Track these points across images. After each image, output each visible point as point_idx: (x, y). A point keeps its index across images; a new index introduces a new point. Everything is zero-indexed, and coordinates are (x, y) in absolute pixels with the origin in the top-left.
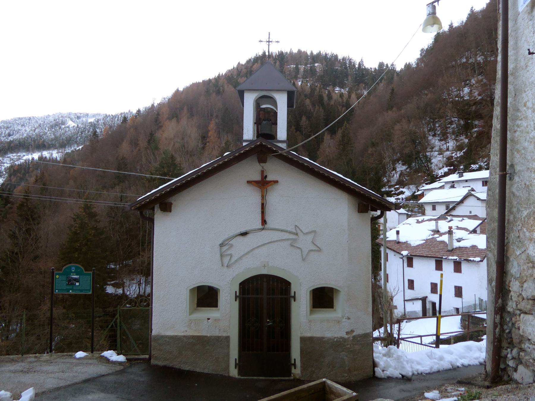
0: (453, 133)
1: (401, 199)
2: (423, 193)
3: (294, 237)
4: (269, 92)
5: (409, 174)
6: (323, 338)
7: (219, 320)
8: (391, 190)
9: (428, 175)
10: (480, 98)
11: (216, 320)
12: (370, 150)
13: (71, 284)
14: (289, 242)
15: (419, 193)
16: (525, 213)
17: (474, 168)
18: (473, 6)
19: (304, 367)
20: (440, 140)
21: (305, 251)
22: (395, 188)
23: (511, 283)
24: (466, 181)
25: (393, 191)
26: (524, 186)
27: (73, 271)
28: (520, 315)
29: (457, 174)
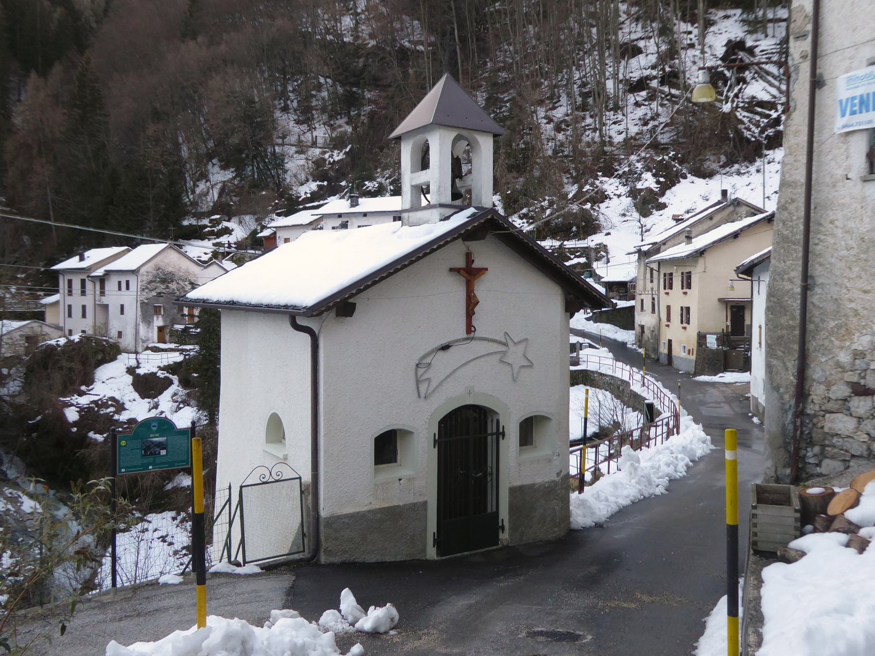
0: (323, 110)
1: (226, 245)
2: (275, 233)
3: (502, 348)
4: (472, 132)
5: (239, 191)
6: (534, 485)
7: (414, 478)
8: (202, 223)
9: (281, 196)
10: (372, 43)
11: (410, 480)
12: (152, 129)
13: (151, 454)
14: (498, 356)
15: (266, 233)
16: (832, 324)
17: (370, 188)
19: (513, 529)
20: (298, 122)
21: (516, 368)
22: (211, 221)
23: (813, 388)
24: (365, 214)
25: (206, 226)
26: (830, 299)
27: (154, 429)
28: (824, 416)
29: (348, 200)
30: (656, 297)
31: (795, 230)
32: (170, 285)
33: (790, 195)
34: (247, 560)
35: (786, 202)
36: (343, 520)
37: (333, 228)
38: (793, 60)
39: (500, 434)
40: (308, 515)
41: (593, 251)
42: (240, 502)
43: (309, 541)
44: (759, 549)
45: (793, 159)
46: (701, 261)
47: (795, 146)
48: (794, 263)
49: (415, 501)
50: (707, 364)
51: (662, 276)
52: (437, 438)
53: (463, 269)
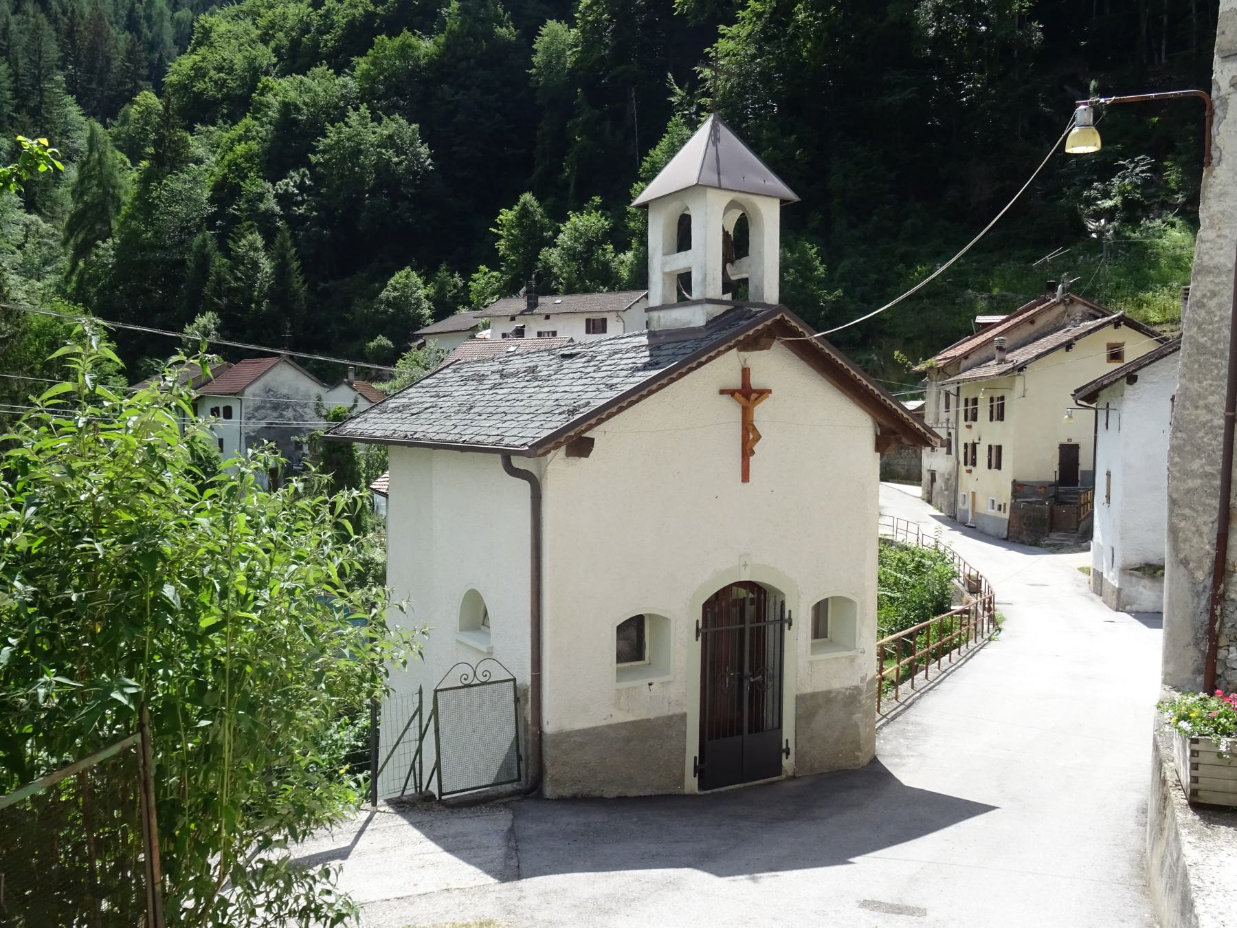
18: (717, 390)
30: (953, 432)
31: (1216, 336)
32: (285, 413)
33: (1211, 287)
34: (444, 791)
35: (1204, 296)
36: (575, 739)
37: (504, 335)
38: (1219, 89)
39: (784, 621)
40: (526, 730)
42: (435, 711)
43: (527, 766)
44: (1202, 801)
45: (1215, 234)
46: (1019, 382)
47: (1219, 215)
48: (1215, 383)
49: (670, 713)
50: (1025, 524)
51: (962, 403)
52: (700, 626)
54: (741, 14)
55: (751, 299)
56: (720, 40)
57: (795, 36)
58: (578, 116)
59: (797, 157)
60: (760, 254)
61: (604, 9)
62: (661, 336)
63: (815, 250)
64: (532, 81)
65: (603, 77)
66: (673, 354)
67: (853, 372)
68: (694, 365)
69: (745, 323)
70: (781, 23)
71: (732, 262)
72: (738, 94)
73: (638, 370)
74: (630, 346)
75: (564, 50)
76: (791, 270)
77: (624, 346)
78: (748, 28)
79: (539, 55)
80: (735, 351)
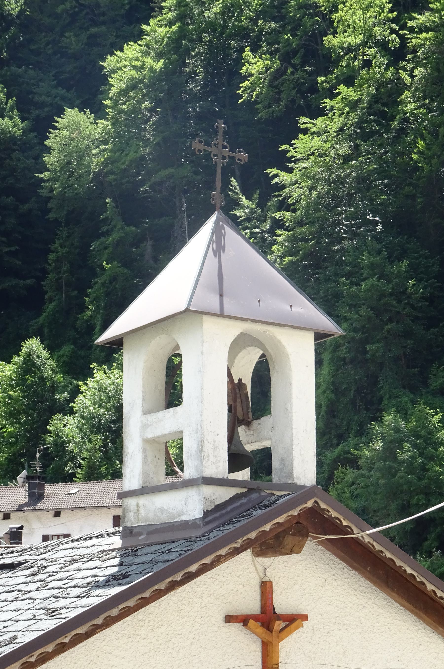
18: (221, 618)
41: (436, 573)
53: (256, 618)
54: (328, 103)
55: (275, 478)
56: (301, 136)
57: (402, 132)
58: (107, 233)
59: (410, 290)
60: (287, 411)
61: (144, 96)
62: (140, 534)
63: (439, 416)
64: (43, 188)
65: (142, 183)
66: (151, 561)
67: (430, 587)
68: (178, 577)
69: (258, 513)
70: (383, 114)
71: (248, 424)
72: (327, 206)
73: (97, 585)
74: (96, 550)
75: (88, 147)
76: (407, 446)
77: (88, 551)
78: (339, 121)
79: (54, 154)
80: (247, 555)
